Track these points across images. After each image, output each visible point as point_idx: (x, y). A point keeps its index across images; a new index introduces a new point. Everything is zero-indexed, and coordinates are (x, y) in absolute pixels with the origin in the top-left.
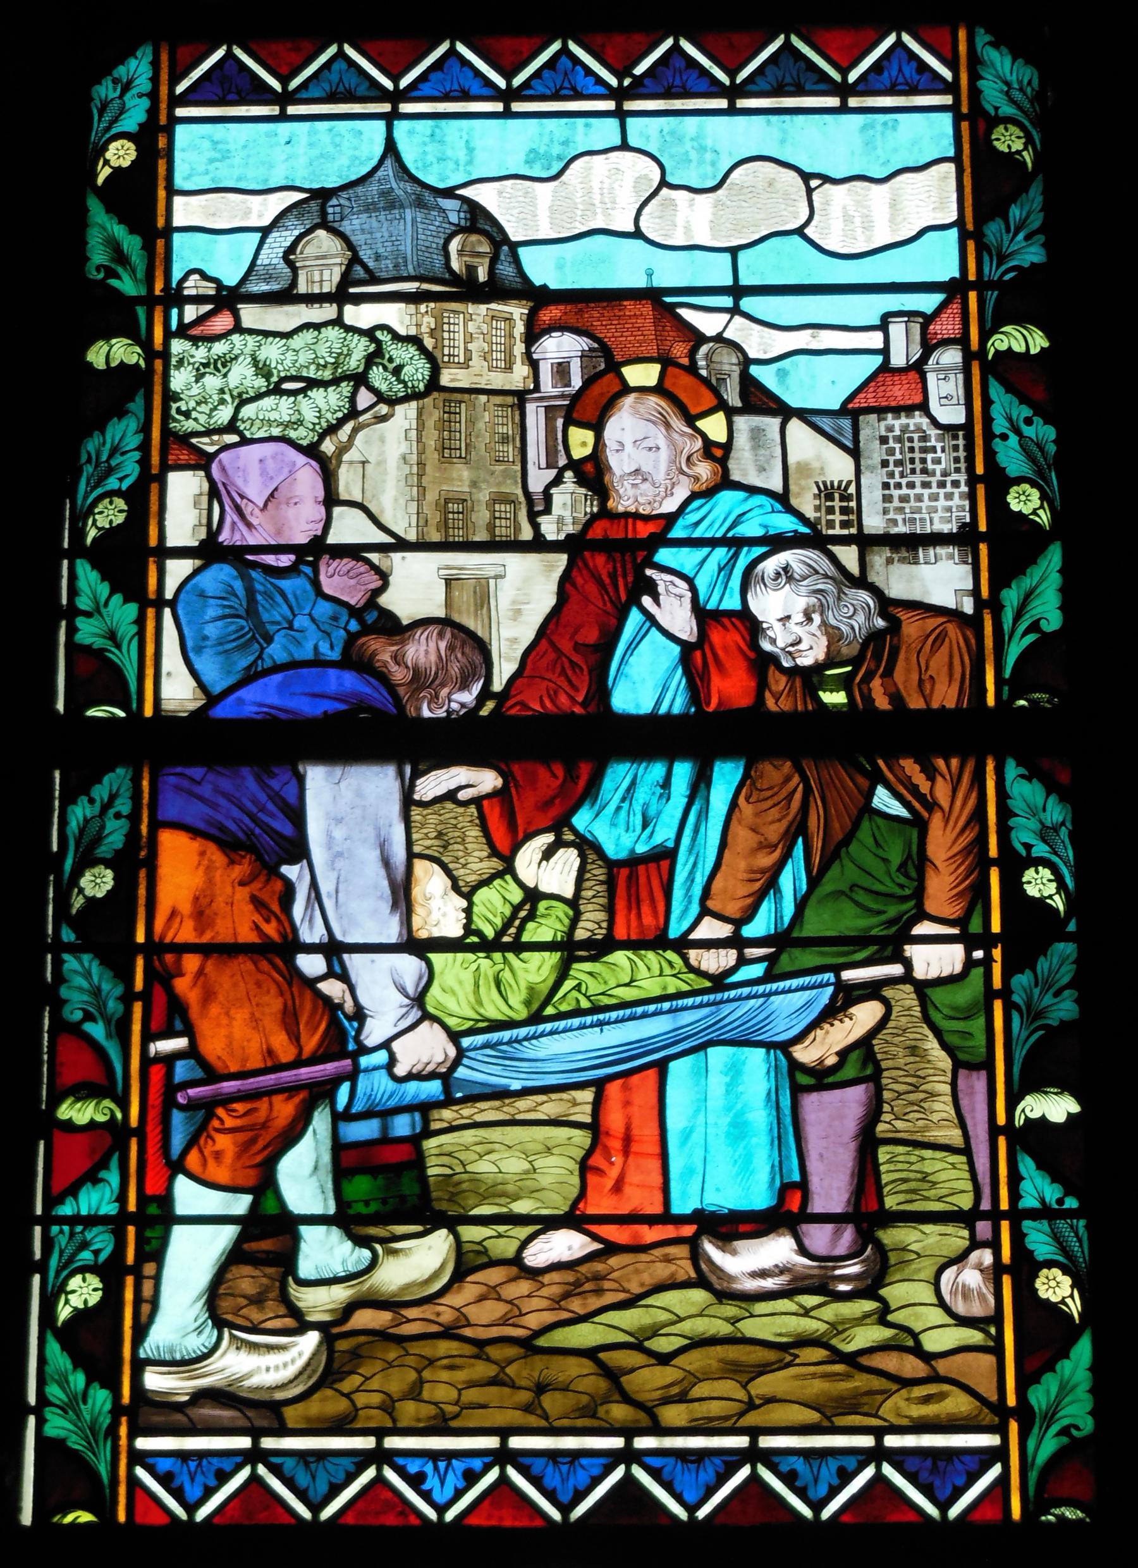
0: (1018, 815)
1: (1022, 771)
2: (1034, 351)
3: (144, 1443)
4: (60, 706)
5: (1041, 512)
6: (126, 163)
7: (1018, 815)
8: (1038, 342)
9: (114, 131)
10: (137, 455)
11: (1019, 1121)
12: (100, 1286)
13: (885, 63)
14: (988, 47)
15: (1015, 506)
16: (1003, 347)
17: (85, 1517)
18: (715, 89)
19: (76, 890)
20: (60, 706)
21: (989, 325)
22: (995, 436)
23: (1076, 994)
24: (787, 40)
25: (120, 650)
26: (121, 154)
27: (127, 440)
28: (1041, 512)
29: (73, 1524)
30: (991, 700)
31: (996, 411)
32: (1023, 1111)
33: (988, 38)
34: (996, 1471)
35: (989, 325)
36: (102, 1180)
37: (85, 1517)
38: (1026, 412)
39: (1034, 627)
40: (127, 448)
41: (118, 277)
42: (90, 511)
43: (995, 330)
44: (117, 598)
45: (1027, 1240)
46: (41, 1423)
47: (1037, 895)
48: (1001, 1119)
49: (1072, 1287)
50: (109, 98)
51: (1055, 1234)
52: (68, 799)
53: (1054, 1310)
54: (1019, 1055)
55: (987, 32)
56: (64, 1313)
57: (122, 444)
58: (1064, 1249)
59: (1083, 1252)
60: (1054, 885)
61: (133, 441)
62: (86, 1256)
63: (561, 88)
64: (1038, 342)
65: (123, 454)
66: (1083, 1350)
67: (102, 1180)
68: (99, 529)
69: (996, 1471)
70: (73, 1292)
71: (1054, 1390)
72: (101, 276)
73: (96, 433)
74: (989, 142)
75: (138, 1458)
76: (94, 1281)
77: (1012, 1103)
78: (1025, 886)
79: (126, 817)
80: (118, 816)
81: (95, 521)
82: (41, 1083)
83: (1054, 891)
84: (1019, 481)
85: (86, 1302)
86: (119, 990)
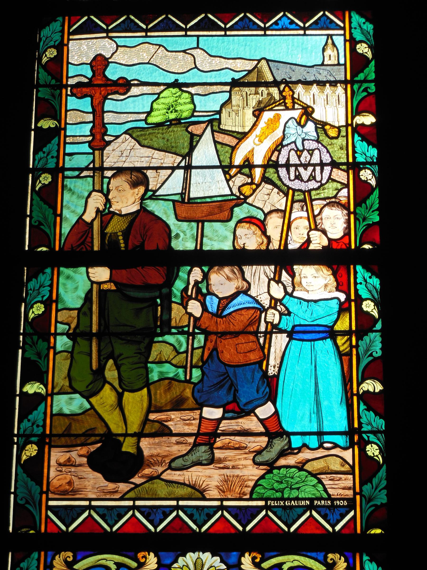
0: (357, 153)
1: (360, 138)
2: (377, 391)
3: (51, 503)
4: (11, 529)
5: (374, 310)
6: (47, 183)
7: (357, 153)
8: (379, 387)
9: (49, 45)
10: (49, 288)
11: (361, 392)
12: (37, 449)
13: (319, 21)
14: (367, 561)
15: (365, 309)
16: (365, 389)
17: (44, 249)
18: (259, 28)
19: (38, 181)
20: (11, 529)
21: (354, 114)
22: (358, 284)
23: (378, 212)
24: (289, 529)
25: (55, 99)
26: (52, 53)
27: (46, 282)
28: (374, 310)
29: (41, 251)
30: (359, 531)
31: (359, 275)
32: (362, 388)
33: (368, 558)
34: (352, 513)
35: (354, 114)
36: (45, 273)
37: (44, 249)
38: (363, 20)
39: (371, 355)
40: (46, 285)
41: (43, 225)
42: (32, 307)
43: (362, 382)
44: (40, 340)
45: (353, 35)
46: (37, 92)
47: (362, 52)
48: (350, 122)
49: (374, 306)
50: (27, 427)
51: (369, 290)
52: (29, 279)
53: (363, 56)
54: (365, 516)
55: (367, 555)
56: (24, 458)
57: (45, 283)
58: (373, 296)
59: (383, 437)
60: (378, 451)
61: (59, 28)
62: (52, 43)
63: (201, 510)
64: (379, 387)
65: (44, 287)
66: (382, 473)
67: (45, 273)
68: (27, 456)
69: (352, 513)
70: (27, 450)
71: (368, 341)
72: (37, 224)
73: (34, 279)
74: (355, 50)
75: (49, 508)
76: (35, 447)
77: (353, 118)
78: (367, 452)
79: (41, 426)
80: (52, 157)
81: (25, 453)
82: (24, 275)
83: (378, 453)
84: (366, 299)
85: (31, 454)
86: (39, 490)
